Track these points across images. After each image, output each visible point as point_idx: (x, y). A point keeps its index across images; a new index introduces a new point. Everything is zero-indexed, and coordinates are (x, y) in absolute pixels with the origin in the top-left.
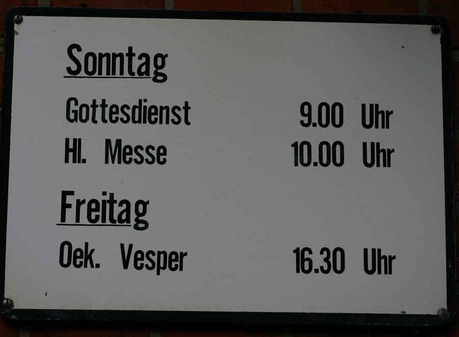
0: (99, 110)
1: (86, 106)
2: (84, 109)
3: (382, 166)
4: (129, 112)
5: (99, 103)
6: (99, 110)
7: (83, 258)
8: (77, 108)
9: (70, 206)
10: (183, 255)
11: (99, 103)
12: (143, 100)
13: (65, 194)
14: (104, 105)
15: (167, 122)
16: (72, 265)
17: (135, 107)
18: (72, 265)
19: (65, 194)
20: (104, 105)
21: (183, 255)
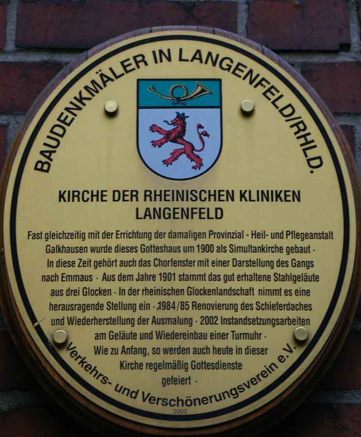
0: (153, 248)
1: (199, 363)
2: (199, 365)
3: (260, 76)
4: (214, 365)
5: (153, 246)
6: (153, 248)
7: (21, 47)
8: (196, 364)
9: (64, 277)
10: (266, 349)
11: (153, 246)
12: (125, 73)
13: (29, 232)
14: (205, 363)
15: (187, 200)
16: (229, 391)
17: (216, 363)
18: (229, 391)
19: (29, 232)
20: (154, 247)
21: (266, 349)
